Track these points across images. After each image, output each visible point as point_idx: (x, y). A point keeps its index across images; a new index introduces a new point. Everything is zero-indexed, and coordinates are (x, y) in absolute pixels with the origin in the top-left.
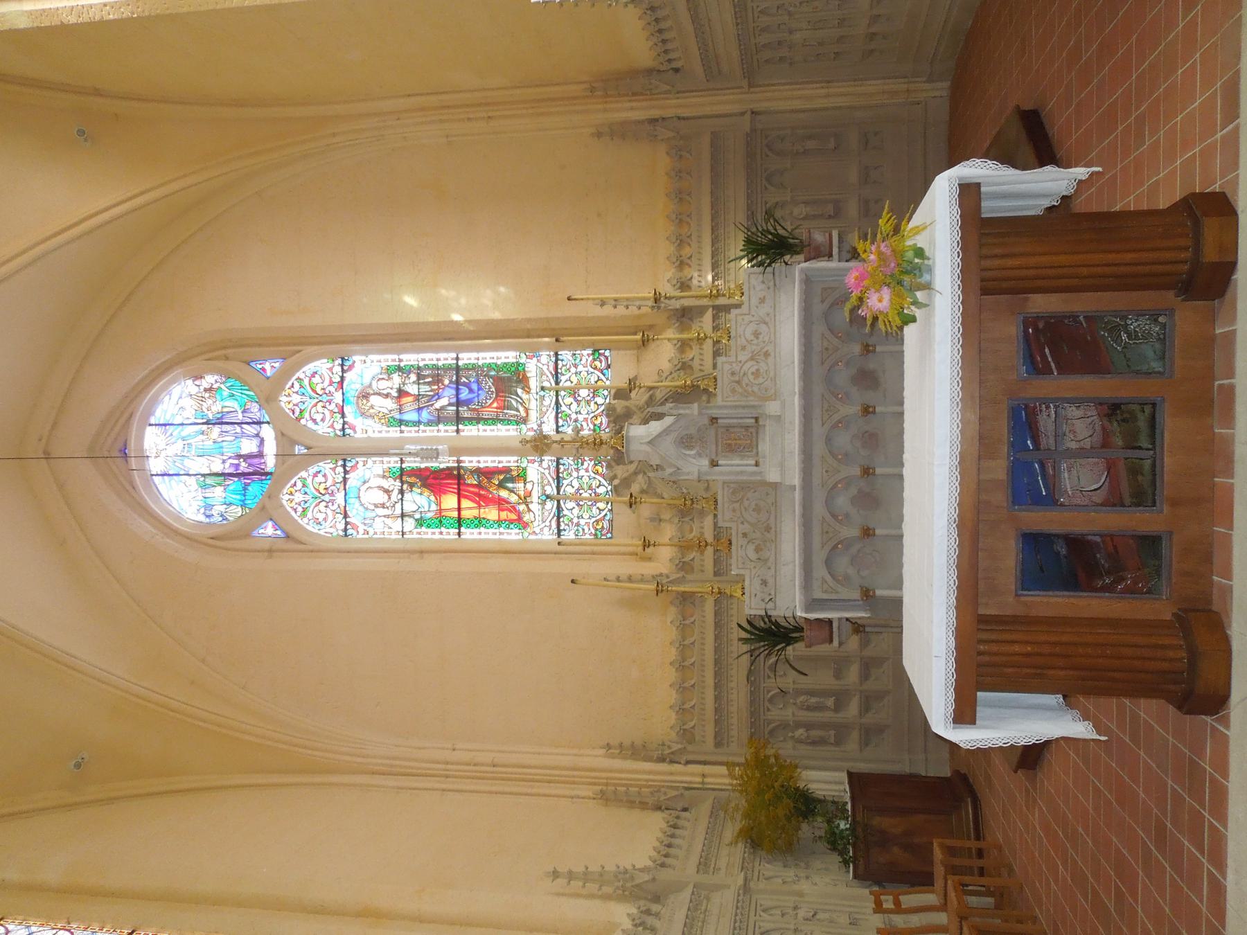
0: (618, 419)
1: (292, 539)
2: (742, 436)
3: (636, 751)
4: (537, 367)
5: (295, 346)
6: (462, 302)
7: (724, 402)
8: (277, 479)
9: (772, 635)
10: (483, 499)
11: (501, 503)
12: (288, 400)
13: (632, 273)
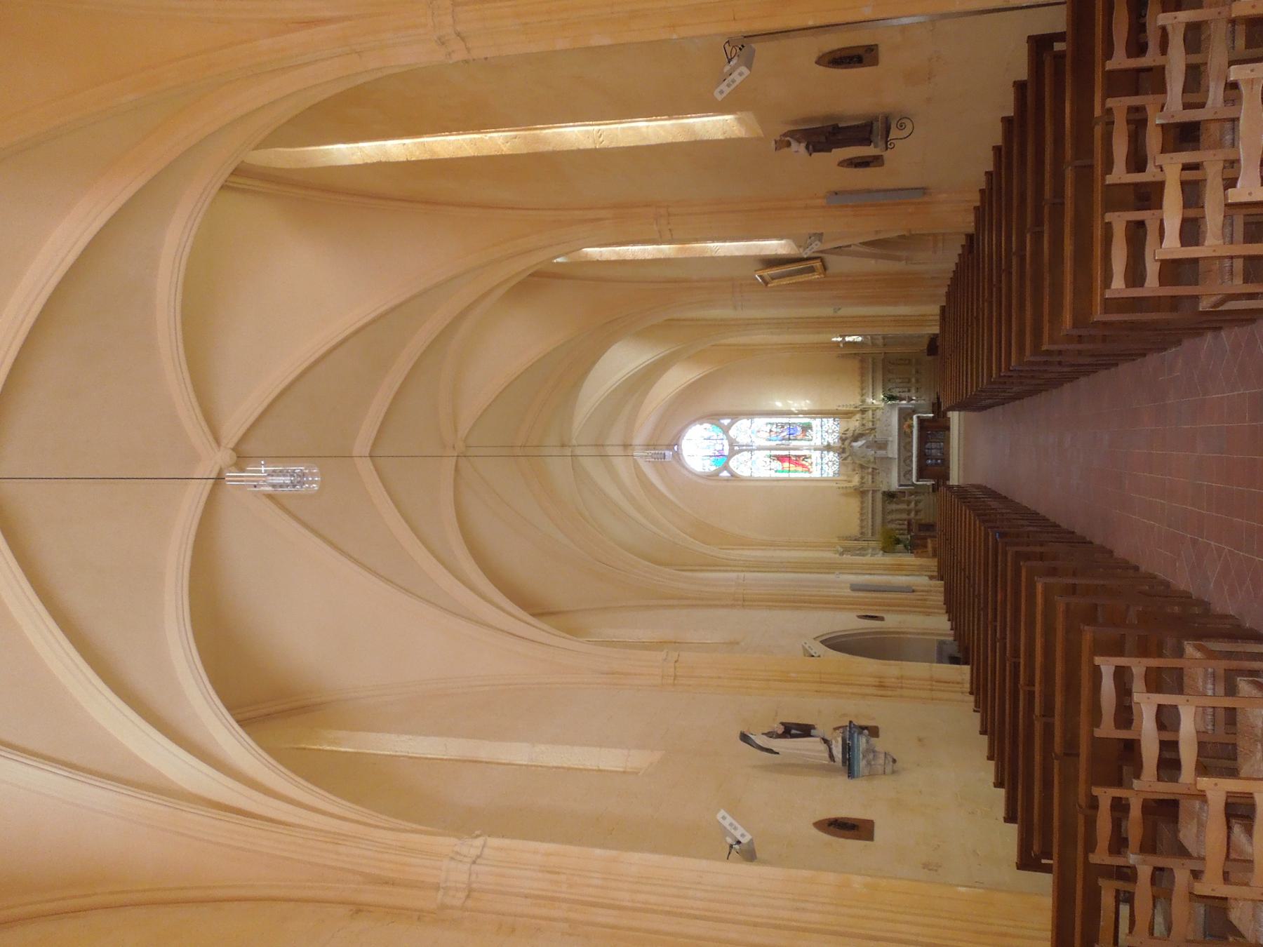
0: (843, 440)
1: (733, 475)
2: (883, 445)
3: (847, 538)
4: (816, 423)
5: (736, 416)
6: (797, 404)
7: (879, 437)
8: (729, 457)
9: (890, 496)
10: (797, 464)
11: (803, 466)
12: (732, 433)
13: (848, 398)
